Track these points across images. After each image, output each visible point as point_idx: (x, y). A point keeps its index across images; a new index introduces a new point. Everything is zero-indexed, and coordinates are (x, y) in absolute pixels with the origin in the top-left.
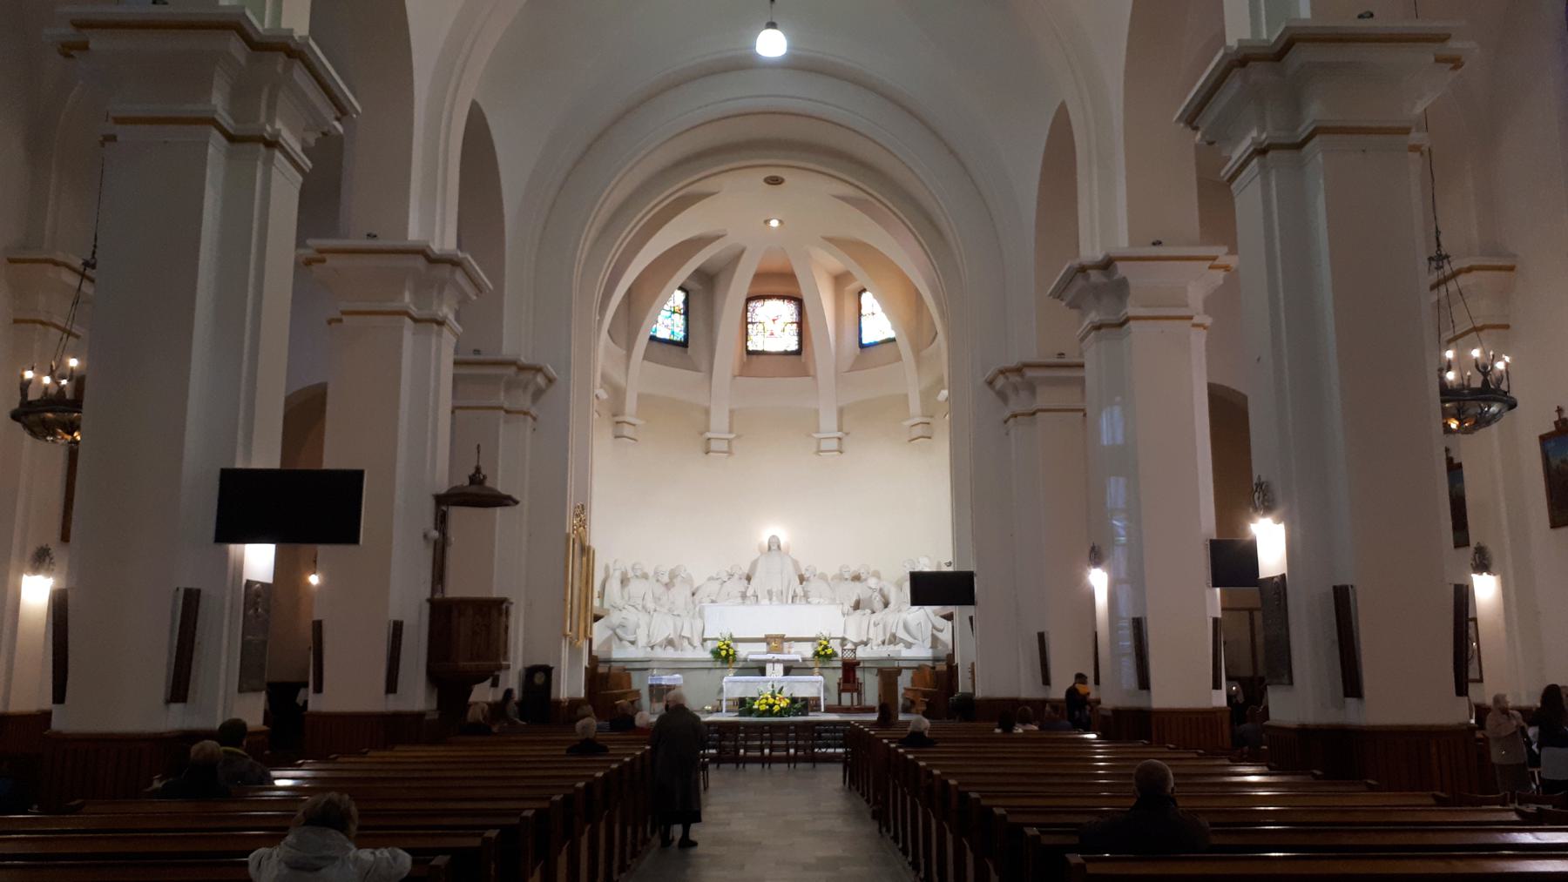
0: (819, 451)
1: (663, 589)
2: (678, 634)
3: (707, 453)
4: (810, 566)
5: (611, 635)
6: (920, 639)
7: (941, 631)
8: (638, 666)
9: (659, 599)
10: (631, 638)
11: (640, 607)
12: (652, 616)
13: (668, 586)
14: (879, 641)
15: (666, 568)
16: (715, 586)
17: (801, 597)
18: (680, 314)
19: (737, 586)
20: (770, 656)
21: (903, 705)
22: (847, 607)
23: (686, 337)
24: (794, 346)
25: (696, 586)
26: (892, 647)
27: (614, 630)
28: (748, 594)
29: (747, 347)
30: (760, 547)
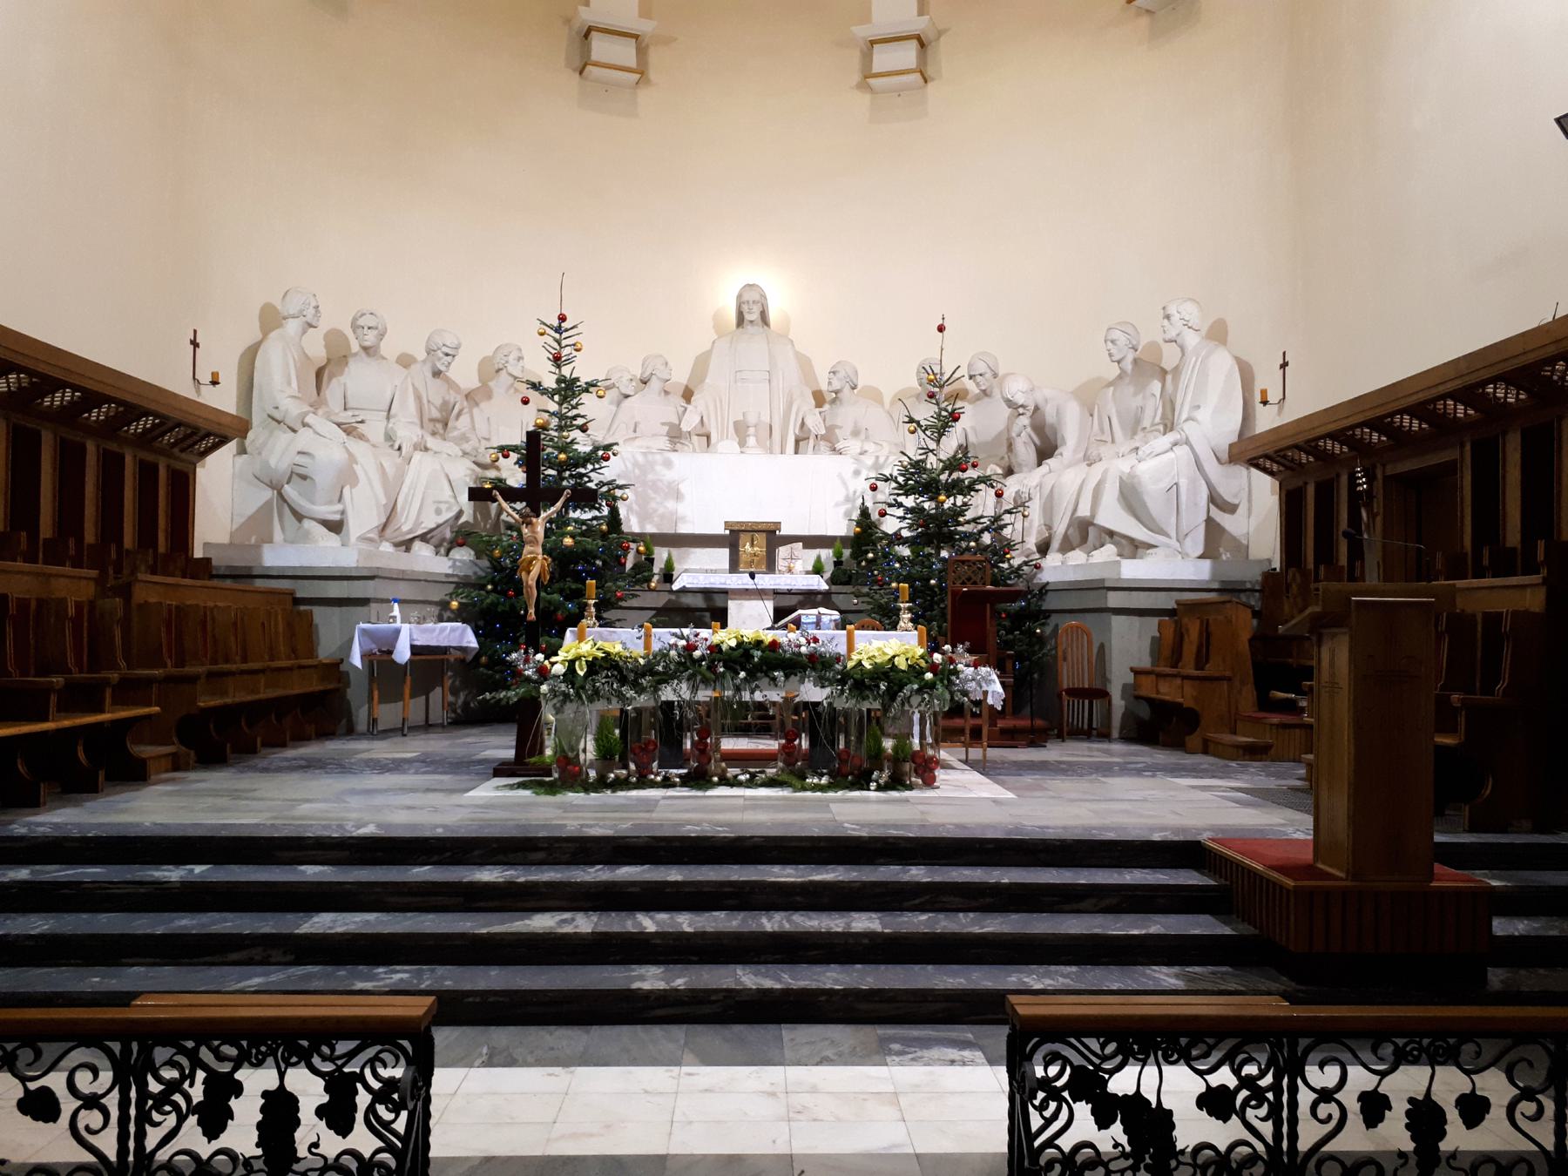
5: (266, 507)
6: (1173, 534)
7: (1231, 509)
10: (330, 512)
11: (374, 428)
21: (1127, 715)
26: (1077, 557)
30: (717, 320)
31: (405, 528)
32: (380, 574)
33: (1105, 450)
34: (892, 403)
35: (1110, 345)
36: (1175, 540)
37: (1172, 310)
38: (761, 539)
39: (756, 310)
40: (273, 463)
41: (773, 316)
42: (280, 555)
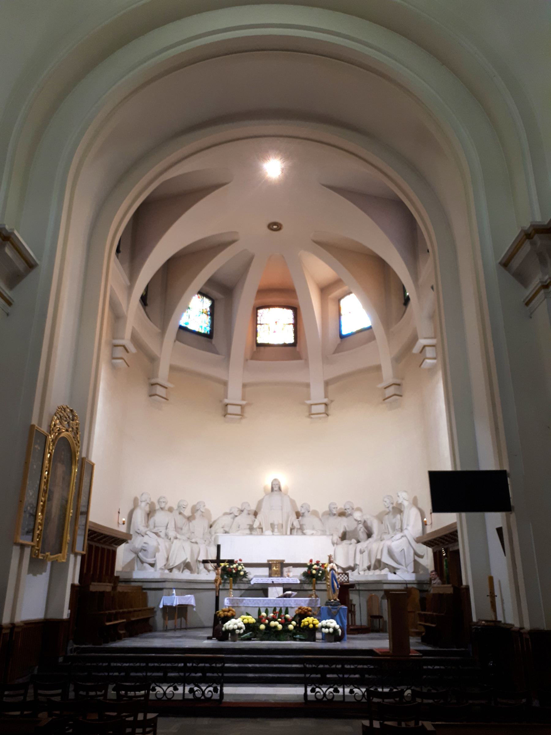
0: (311, 414)
1: (185, 520)
2: (195, 559)
3: (225, 416)
4: (304, 504)
5: (133, 560)
6: (404, 564)
7: (421, 557)
8: (154, 585)
9: (182, 529)
10: (151, 561)
11: (162, 534)
12: (172, 543)
13: (189, 519)
14: (366, 565)
15: (190, 502)
16: (229, 518)
17: (298, 529)
18: (208, 315)
19: (244, 520)
20: (269, 580)
22: (336, 538)
23: (212, 331)
24: (292, 341)
25: (213, 520)
26: (377, 572)
27: (136, 554)
28: (255, 526)
29: (256, 341)
30: (265, 489)
31: (171, 565)
32: (167, 580)
33: (385, 536)
35: (385, 503)
36: (405, 567)
37: (399, 494)
38: (279, 565)
39: (277, 486)
41: (283, 487)
42: (138, 575)
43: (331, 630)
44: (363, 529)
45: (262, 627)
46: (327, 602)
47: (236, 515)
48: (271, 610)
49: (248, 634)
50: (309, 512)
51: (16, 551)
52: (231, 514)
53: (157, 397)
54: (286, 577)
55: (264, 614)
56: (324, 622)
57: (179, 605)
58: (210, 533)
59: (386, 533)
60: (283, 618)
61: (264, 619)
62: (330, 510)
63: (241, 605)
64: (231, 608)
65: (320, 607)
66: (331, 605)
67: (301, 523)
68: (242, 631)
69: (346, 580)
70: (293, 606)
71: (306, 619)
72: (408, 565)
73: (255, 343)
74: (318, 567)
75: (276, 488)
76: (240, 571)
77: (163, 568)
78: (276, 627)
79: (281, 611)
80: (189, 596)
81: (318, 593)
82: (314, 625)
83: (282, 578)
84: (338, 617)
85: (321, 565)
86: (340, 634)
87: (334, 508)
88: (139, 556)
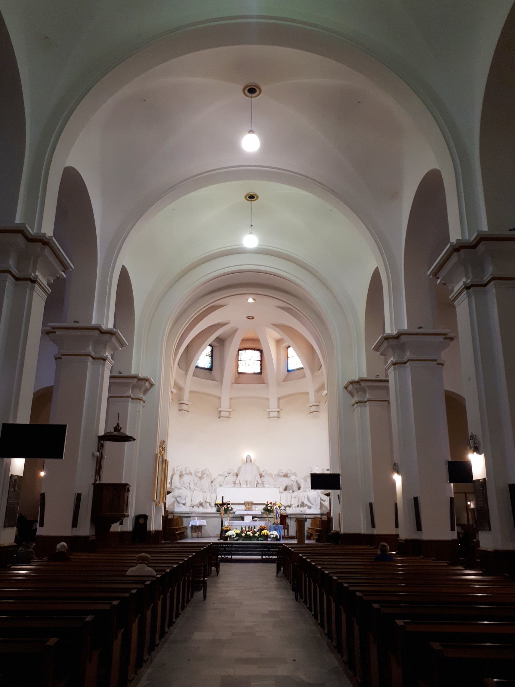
1: (198, 479)
5: (174, 502)
7: (324, 501)
9: (197, 484)
11: (188, 488)
19: (231, 479)
21: (307, 535)
22: (282, 489)
23: (212, 366)
26: (302, 509)
28: (237, 482)
29: (238, 371)
34: (275, 476)
35: (307, 471)
37: (315, 468)
39: (250, 460)
40: (176, 495)
41: (252, 459)
43: (275, 536)
44: (296, 485)
45: (243, 535)
46: (273, 524)
47: (226, 476)
48: (247, 527)
49: (236, 538)
50: (267, 474)
51: (153, 502)
52: (223, 475)
53: (183, 411)
54: (253, 511)
55: (244, 529)
56: (272, 533)
57: (199, 525)
58: (212, 486)
59: (308, 487)
60: (253, 531)
61: (244, 531)
62: (279, 474)
63: (233, 525)
64: (229, 526)
65: (270, 526)
66: (275, 525)
67: (263, 481)
68: (234, 536)
69: (285, 512)
70: (257, 525)
71: (263, 531)
72: (317, 505)
73: (237, 372)
74: (271, 505)
75: (248, 460)
76: (229, 507)
77: (190, 506)
78: (249, 535)
79: (252, 527)
80: (203, 520)
81: (270, 519)
82: (267, 534)
83: (252, 511)
84: (278, 530)
85: (273, 504)
86: (279, 538)
87: (281, 473)
88: (177, 500)
